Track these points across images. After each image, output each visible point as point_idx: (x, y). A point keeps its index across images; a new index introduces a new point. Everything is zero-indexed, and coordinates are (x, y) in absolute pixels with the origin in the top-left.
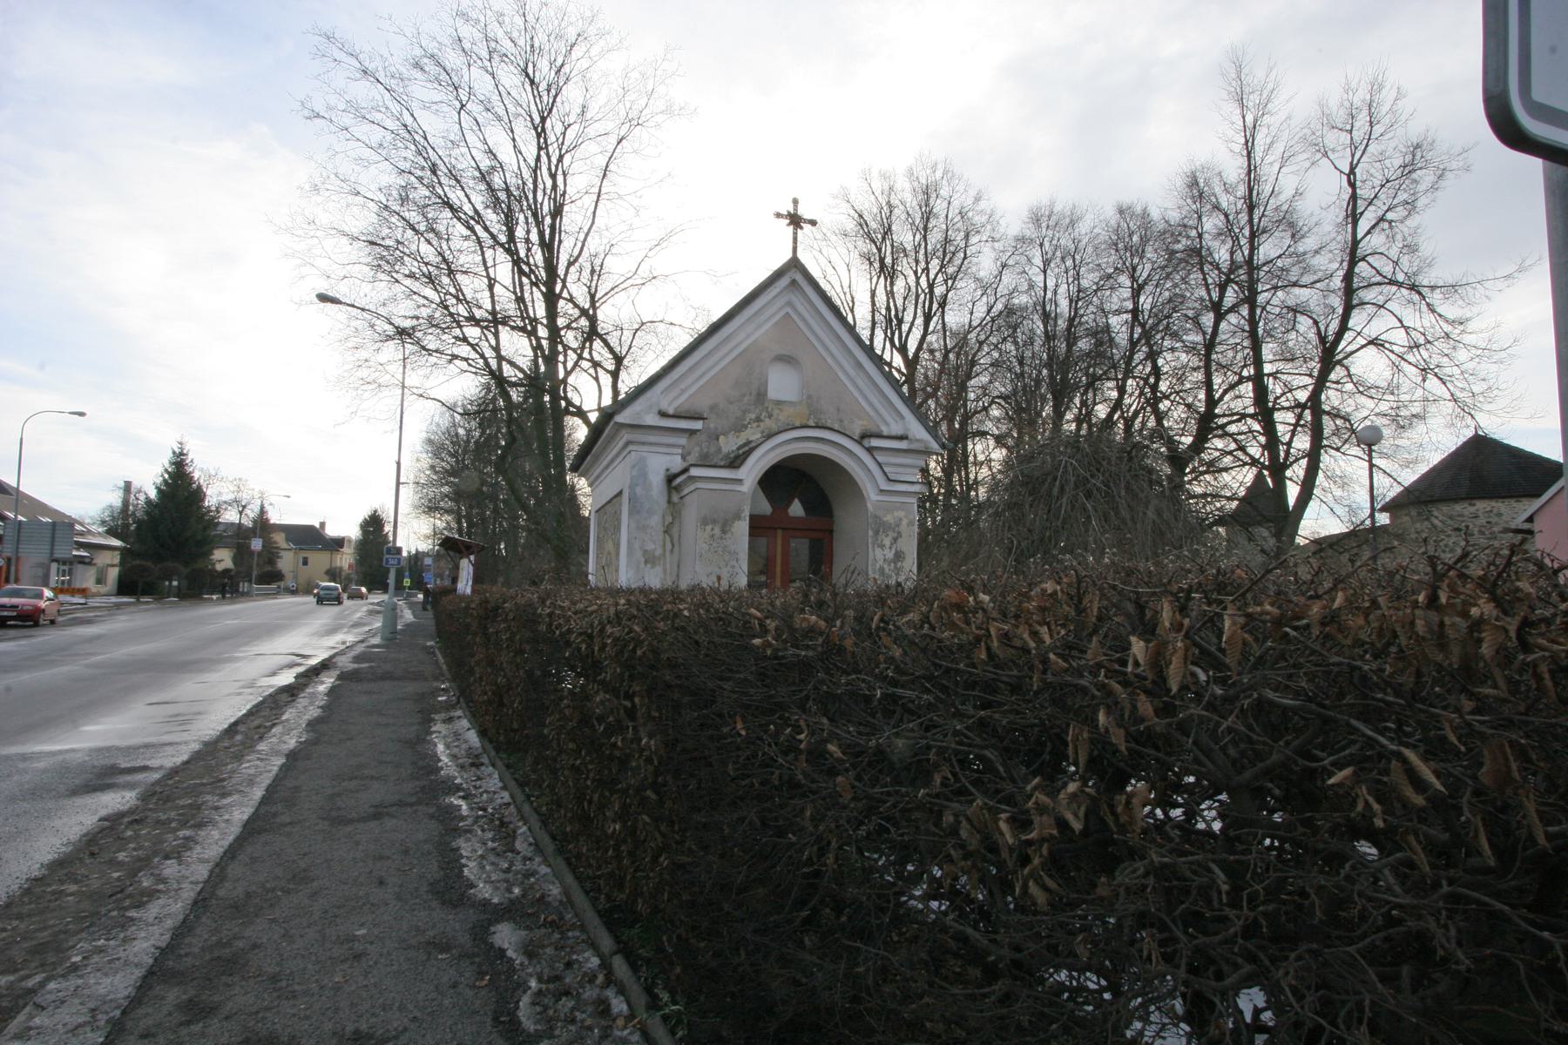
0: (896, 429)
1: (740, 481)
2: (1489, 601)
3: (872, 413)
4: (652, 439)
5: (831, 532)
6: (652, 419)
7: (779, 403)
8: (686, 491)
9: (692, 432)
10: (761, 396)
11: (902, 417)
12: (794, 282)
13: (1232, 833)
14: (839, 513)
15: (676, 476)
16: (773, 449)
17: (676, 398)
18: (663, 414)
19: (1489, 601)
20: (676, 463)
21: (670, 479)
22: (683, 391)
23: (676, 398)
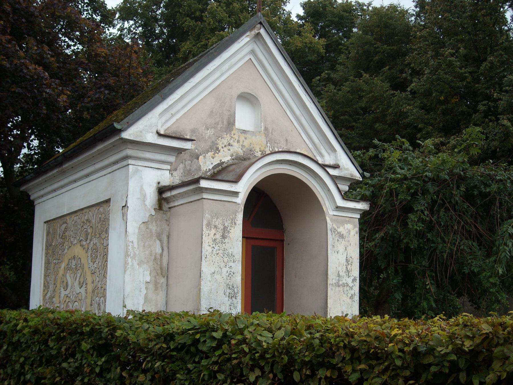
0: (329, 160)
1: (236, 194)
2: (10, 269)
3: (311, 146)
4: (148, 155)
5: (283, 241)
6: (151, 138)
7: (244, 132)
8: (172, 205)
9: (179, 151)
10: (231, 124)
11: (334, 150)
12: (259, 34)
13: (63, 371)
14: (288, 226)
15: (171, 188)
16: (260, 168)
17: (167, 121)
18: (159, 134)
19: (10, 269)
20: (166, 178)
21: (161, 190)
22: (173, 115)
23: (167, 121)
